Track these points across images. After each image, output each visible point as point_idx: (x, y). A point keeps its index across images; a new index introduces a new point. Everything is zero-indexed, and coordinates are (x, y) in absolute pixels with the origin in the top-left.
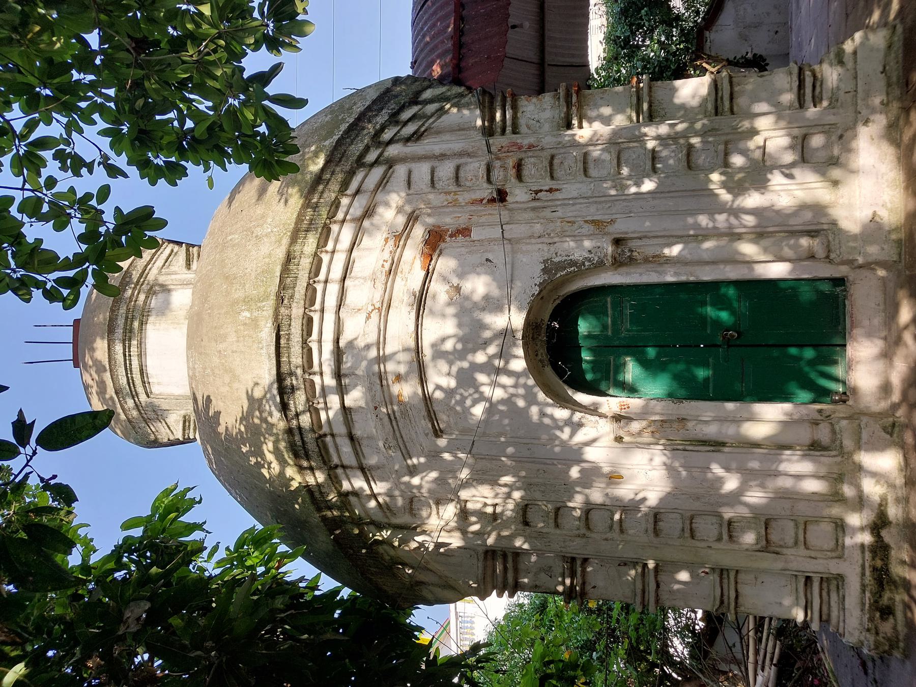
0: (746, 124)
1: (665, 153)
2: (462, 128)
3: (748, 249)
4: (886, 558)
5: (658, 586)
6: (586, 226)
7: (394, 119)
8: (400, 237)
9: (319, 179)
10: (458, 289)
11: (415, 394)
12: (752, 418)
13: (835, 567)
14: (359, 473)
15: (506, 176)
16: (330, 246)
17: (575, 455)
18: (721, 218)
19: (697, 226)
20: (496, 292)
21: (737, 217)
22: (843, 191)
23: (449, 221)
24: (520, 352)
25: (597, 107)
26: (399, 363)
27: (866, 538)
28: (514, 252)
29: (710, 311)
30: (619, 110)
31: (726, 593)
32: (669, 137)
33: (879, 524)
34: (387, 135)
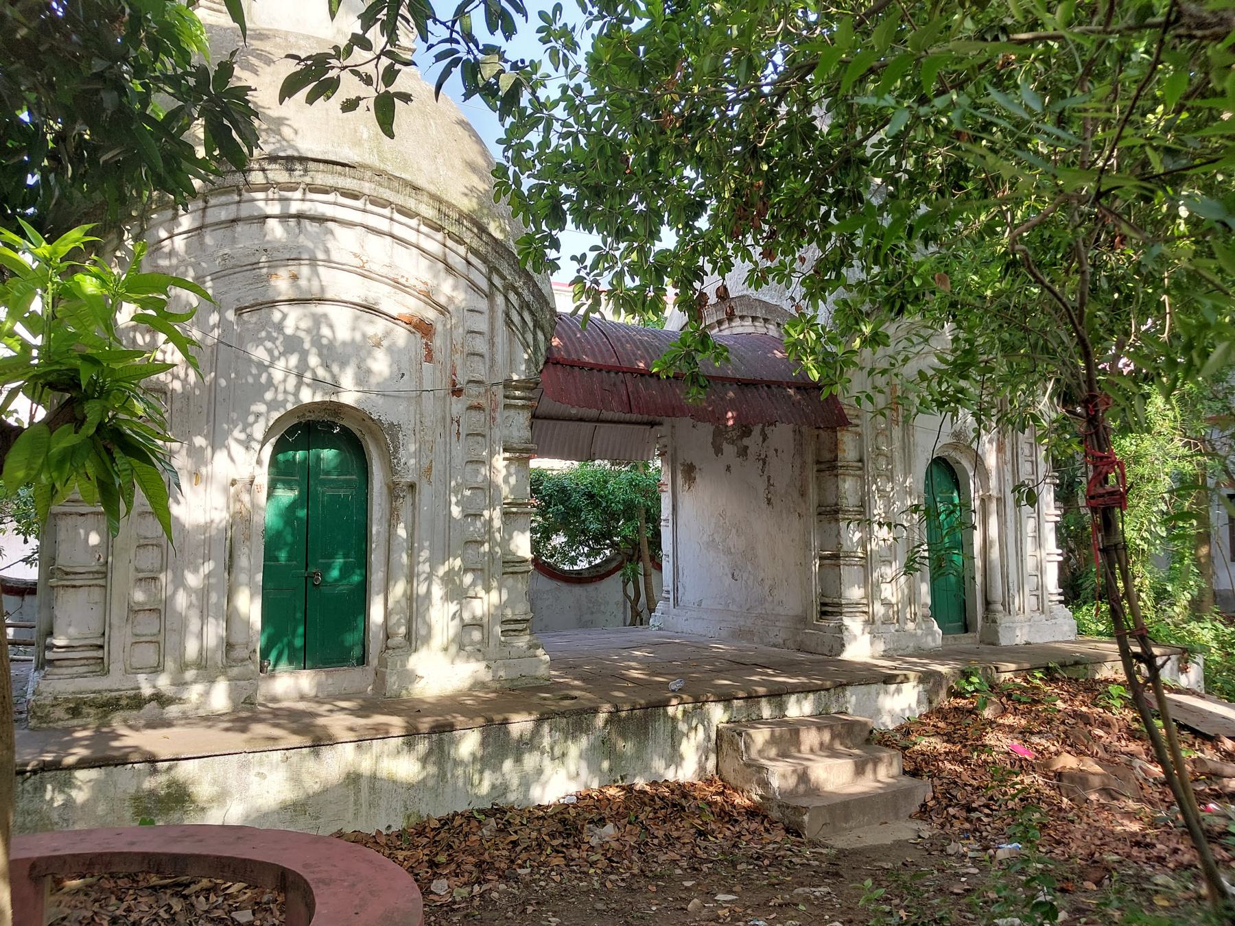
0: (495, 584)
1: (479, 524)
2: (512, 363)
3: (399, 589)
4: (129, 707)
5: (82, 515)
7: (525, 305)
8: (428, 297)
9: (483, 230)
10: (378, 345)
11: (279, 294)
12: (252, 596)
13: (116, 668)
14: (196, 225)
16: (424, 229)
17: (217, 442)
18: (426, 568)
19: (421, 549)
20: (374, 380)
21: (426, 579)
22: (441, 654)
23: (438, 342)
24: (318, 398)
25: (517, 473)
26: (309, 280)
27: (147, 691)
28: (409, 398)
29: (339, 561)
30: (512, 491)
32: (491, 527)
33: (161, 700)
34: (512, 297)
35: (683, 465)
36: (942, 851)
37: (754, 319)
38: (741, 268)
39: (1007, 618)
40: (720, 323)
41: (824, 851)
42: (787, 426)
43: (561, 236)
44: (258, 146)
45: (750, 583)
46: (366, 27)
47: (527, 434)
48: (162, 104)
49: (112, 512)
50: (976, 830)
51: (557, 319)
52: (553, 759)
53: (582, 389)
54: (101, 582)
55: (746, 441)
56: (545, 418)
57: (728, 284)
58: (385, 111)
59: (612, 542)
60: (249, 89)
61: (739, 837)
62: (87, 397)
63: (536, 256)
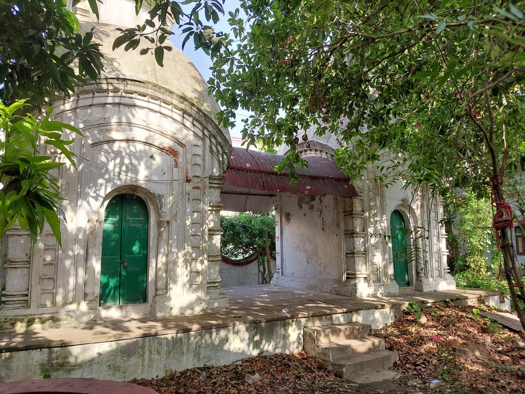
5: (20, 235)
6: (175, 211)
7: (218, 143)
13: (33, 305)
14: (74, 106)
15: (195, 183)
23: (180, 160)
31: (17, 263)
34: (213, 140)
36: (405, 384)
37: (316, 150)
38: (313, 127)
39: (426, 280)
41: (353, 385)
42: (332, 194)
43: (236, 112)
44: (103, 70)
45: (315, 265)
46: (152, 17)
47: (219, 199)
48: (60, 51)
49: (34, 233)
50: (419, 374)
52: (234, 333)
54: (28, 266)
55: (313, 203)
56: (225, 193)
57: (307, 133)
58: (159, 54)
60: (99, 45)
61: (315, 379)
62: (23, 178)
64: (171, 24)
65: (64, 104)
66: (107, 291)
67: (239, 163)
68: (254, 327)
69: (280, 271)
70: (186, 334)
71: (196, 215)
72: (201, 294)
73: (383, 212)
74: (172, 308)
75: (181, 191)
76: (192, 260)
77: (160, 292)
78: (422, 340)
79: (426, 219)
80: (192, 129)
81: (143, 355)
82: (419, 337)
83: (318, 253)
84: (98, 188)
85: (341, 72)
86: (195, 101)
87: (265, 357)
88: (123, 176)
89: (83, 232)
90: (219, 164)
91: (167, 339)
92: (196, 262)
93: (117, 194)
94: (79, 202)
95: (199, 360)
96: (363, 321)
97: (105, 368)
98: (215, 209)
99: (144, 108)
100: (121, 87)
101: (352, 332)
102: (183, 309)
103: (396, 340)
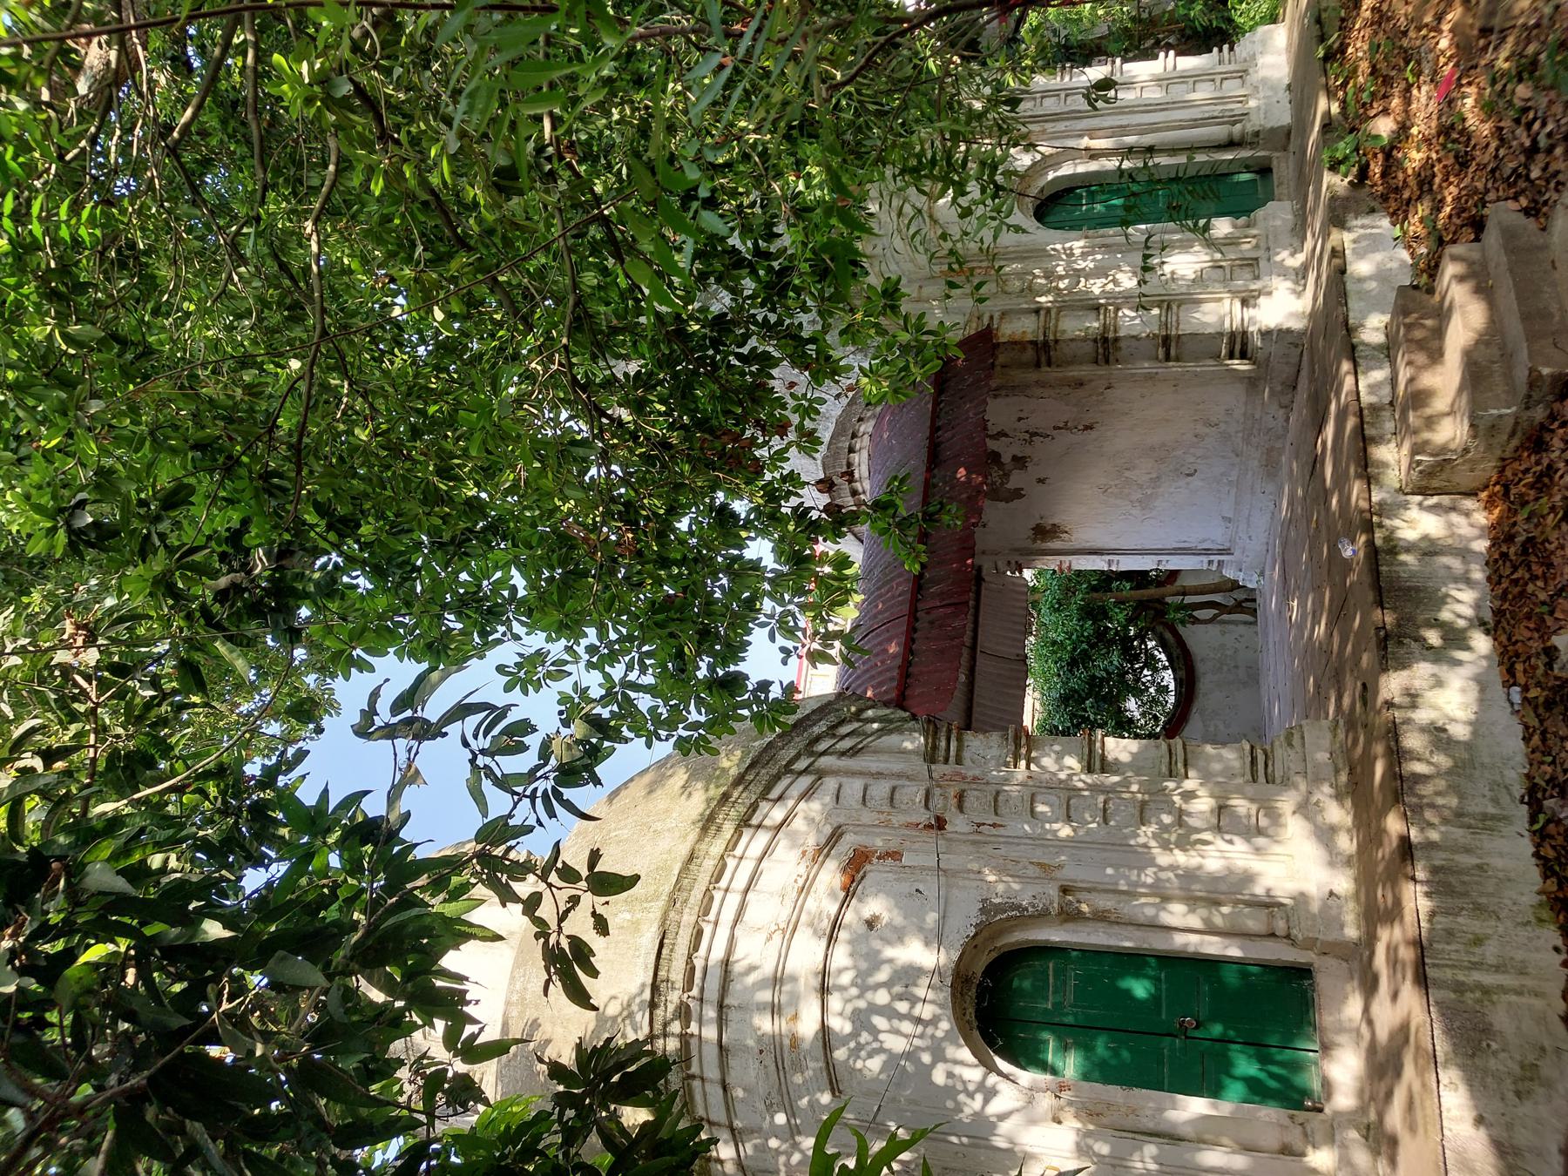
6: (1031, 867)
23: (879, 843)
28: (949, 886)
34: (822, 746)
35: (1034, 541)
38: (796, 462)
39: (1253, 117)
40: (854, 493)
42: (986, 408)
47: (995, 737)
51: (849, 693)
52: (1414, 706)
53: (937, 666)
57: (812, 479)
58: (609, 884)
59: (1136, 637)
63: (780, 711)
64: (531, 847)
65: (721, 1162)
66: (1273, 1084)
67: (889, 674)
68: (1393, 647)
69: (1216, 558)
70: (1417, 854)
71: (1041, 808)
72: (1287, 803)
73: (1038, 254)
74: (1331, 894)
75: (971, 848)
76: (1181, 826)
77: (1280, 927)
78: (1450, 131)
79: (1061, 126)
80: (791, 803)
81: (1486, 991)
82: (1441, 139)
83: (1163, 445)
84: (959, 1087)
85: (654, 387)
86: (715, 792)
87: (1498, 613)
88: (926, 1012)
89: (1090, 1141)
90: (891, 732)
91: (1432, 914)
92: (1189, 814)
93: (976, 1033)
94: (1000, 1143)
95: (1505, 818)
96: (1383, 313)
97: (1526, 1109)
98: (1023, 751)
99: (732, 936)
100: (674, 997)
101: (1421, 345)
102: (1334, 859)
103: (1448, 209)
